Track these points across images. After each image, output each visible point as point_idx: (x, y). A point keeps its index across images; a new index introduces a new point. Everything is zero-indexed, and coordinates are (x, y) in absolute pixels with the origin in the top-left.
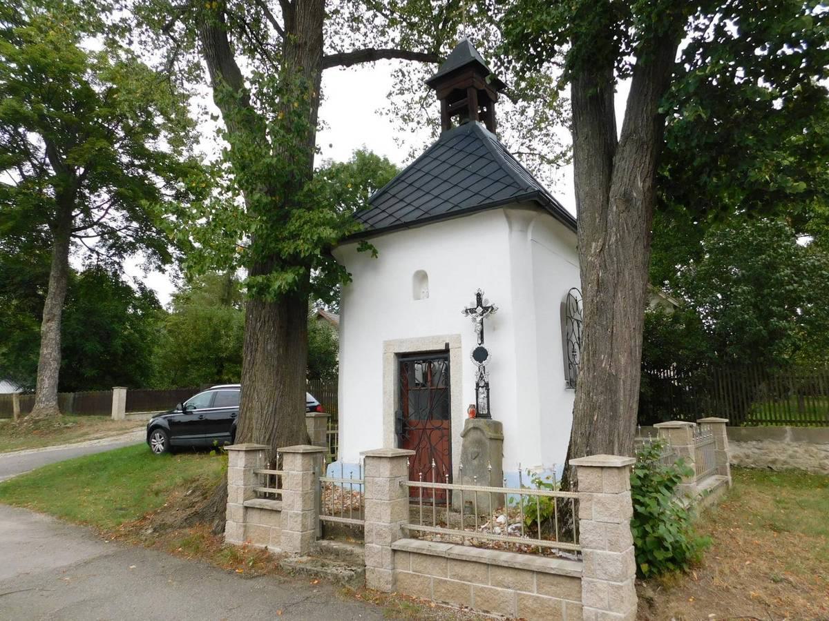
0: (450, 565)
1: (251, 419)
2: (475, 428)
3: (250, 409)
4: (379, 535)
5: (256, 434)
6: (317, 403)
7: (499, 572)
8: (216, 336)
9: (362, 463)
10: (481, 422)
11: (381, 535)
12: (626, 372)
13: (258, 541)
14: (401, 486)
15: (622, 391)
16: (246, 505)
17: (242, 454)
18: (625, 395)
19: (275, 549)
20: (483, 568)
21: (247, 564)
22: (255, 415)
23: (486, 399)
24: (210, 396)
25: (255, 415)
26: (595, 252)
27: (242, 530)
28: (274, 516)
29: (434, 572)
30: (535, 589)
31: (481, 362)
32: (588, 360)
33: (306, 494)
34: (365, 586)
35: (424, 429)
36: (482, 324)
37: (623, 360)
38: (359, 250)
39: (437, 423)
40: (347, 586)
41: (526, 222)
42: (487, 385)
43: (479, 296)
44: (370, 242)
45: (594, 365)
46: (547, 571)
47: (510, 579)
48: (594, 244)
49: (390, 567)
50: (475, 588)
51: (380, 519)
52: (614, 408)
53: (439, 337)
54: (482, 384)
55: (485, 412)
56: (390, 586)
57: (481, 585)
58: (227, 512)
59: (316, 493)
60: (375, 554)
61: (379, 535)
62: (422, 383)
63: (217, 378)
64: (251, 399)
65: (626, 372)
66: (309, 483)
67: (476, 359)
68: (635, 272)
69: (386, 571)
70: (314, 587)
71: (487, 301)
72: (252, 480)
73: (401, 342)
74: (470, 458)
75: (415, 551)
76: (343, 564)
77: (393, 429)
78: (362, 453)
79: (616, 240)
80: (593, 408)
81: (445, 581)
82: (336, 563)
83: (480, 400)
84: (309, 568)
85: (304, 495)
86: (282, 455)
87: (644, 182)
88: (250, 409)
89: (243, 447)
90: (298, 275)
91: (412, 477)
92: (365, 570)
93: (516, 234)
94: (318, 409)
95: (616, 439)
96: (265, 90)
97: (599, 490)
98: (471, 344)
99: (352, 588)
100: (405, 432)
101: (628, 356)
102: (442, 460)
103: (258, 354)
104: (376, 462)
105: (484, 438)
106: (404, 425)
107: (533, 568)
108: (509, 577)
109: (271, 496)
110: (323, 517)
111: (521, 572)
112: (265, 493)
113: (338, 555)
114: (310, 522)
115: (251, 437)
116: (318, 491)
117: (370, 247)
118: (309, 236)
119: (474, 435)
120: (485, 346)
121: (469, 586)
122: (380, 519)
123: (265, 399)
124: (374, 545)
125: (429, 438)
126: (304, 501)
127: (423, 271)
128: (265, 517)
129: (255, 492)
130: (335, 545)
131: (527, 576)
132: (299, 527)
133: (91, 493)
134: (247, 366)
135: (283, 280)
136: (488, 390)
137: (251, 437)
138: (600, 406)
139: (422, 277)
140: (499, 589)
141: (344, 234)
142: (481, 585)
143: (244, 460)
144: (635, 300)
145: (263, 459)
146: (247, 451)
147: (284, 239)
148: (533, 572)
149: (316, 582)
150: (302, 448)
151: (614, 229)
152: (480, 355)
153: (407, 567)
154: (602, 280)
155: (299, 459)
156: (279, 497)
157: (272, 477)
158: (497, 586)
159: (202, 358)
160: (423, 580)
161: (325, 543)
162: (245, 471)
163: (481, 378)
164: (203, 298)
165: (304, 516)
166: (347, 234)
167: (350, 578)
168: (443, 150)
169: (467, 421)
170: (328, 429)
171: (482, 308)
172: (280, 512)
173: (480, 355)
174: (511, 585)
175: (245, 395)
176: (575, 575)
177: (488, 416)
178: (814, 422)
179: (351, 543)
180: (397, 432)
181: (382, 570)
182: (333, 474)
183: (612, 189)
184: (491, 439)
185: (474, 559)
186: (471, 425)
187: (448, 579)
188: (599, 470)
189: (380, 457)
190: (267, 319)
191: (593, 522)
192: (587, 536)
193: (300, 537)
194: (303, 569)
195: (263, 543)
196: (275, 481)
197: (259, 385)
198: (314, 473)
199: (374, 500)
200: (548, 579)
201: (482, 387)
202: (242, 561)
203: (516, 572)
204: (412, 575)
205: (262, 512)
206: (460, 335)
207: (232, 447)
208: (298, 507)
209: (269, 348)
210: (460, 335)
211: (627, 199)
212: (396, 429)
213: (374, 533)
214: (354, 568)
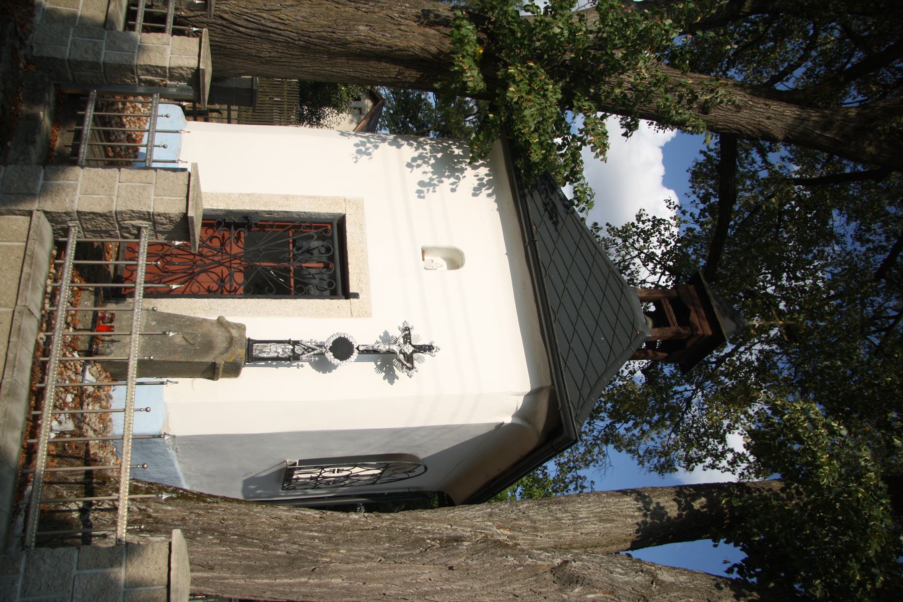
9: (181, 166)
18: (283, 585)
23: (275, 355)
31: (331, 349)
43: (429, 348)
51: (86, 193)
52: (265, 570)
62: (301, 255)
65: (319, 586)
67: (335, 342)
71: (422, 360)
77: (233, 207)
78: (195, 166)
83: (273, 347)
86: (198, 34)
96: (591, 36)
105: (216, 352)
112: (137, 6)
122: (86, 193)
123: (285, 17)
127: (462, 265)
132: (77, 56)
133: (313, 547)
152: (343, 348)
157: (162, 19)
180: (230, 213)
182: (170, 114)
191: (75, 572)
192: (48, 561)
193: (59, 56)
201: (293, 350)
206: (370, 315)
209: (361, 28)
210: (370, 315)
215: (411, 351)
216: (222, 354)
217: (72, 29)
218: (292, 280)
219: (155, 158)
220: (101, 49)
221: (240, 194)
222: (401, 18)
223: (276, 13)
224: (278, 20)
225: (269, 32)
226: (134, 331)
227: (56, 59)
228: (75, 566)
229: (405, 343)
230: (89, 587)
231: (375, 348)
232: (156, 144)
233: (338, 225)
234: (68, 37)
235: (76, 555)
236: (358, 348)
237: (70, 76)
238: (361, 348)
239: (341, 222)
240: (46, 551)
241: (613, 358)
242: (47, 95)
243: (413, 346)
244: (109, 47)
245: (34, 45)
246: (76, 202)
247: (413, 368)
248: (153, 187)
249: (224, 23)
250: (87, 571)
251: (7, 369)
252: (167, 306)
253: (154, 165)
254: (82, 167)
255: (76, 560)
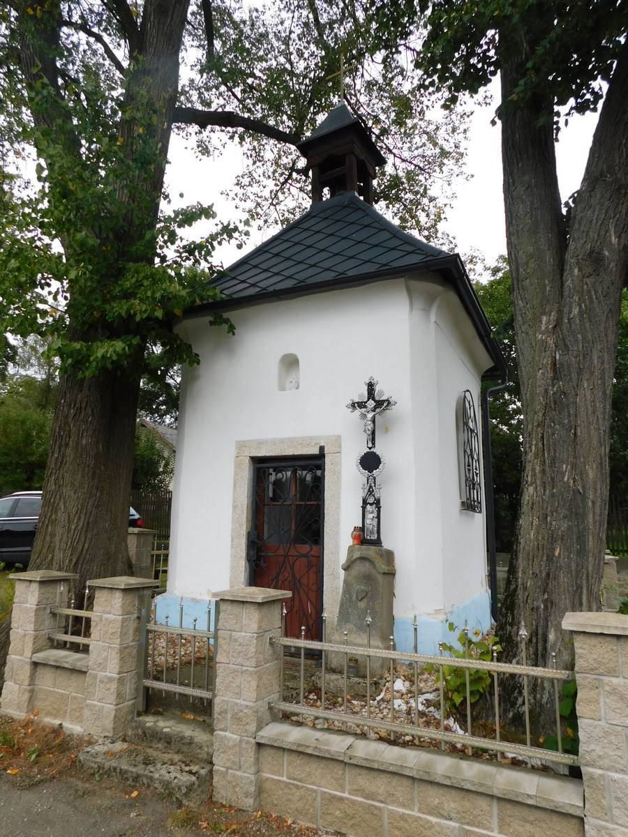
0: (349, 774)
1: (53, 535)
2: (362, 559)
3: (53, 523)
4: (237, 719)
5: (59, 555)
6: (137, 516)
7: (432, 792)
8: (28, 440)
10: (371, 551)
11: (240, 719)
12: (595, 490)
13: (49, 714)
14: (271, 644)
15: (591, 516)
16: (34, 659)
17: (35, 586)
18: (595, 522)
19: (74, 728)
20: (406, 782)
21: (27, 758)
22: (59, 531)
24: (11, 503)
25: (59, 531)
26: (547, 328)
27: (27, 696)
28: (75, 680)
29: (323, 783)
30: (495, 821)
31: (371, 471)
32: (543, 472)
33: (125, 648)
34: (211, 798)
35: (286, 556)
36: (374, 421)
37: (591, 474)
38: (211, 323)
39: (305, 548)
40: (185, 802)
41: (430, 299)
42: (377, 503)
43: (371, 387)
44: (225, 315)
45: (553, 479)
46: (520, 800)
47: (453, 805)
48: (544, 319)
49: (253, 770)
50: (391, 812)
51: (239, 695)
53: (311, 438)
54: (371, 500)
55: (375, 537)
56: (251, 801)
57: (401, 810)
58: (7, 669)
59: (140, 646)
60: (229, 744)
61: (237, 719)
62: (286, 497)
63: (27, 484)
64: (55, 510)
65: (595, 490)
66: (131, 632)
67: (364, 468)
68: (606, 356)
69: (246, 775)
70: (132, 805)
71: (382, 393)
72: (47, 623)
73: (260, 443)
74: (354, 598)
75: (294, 748)
76: (177, 758)
77: (244, 554)
78: (214, 595)
79: (580, 311)
80: (553, 540)
81: (341, 799)
82: (167, 757)
83: (368, 521)
84: (124, 767)
85: (122, 651)
87: (619, 237)
88: (53, 523)
89: (37, 575)
90: (129, 346)
91: (290, 631)
92: (211, 771)
93: (418, 314)
94: (139, 522)
95: (584, 582)
97: (612, 672)
98: (354, 449)
99: (192, 804)
100: (261, 563)
101: (597, 468)
102: (307, 595)
103: (69, 451)
104: (236, 609)
105: (374, 572)
106: (259, 550)
107: (496, 792)
108: (451, 803)
109: (76, 648)
110: (150, 683)
111: (471, 795)
112: (65, 642)
113: (169, 743)
114: (129, 689)
115: (52, 559)
116: (143, 629)
117: (227, 321)
118: (149, 294)
119: (359, 568)
120: (377, 450)
121: (379, 809)
122: (239, 695)
123: (75, 509)
124: (228, 734)
125: (292, 569)
126: (122, 659)
128: (62, 678)
129: (51, 639)
130: (166, 725)
131: (483, 803)
134: (53, 466)
135: (109, 349)
136: (379, 508)
137: (52, 559)
138: (563, 536)
139: (290, 363)
140: (433, 819)
141: (194, 301)
142: (401, 810)
143: (37, 594)
144: (604, 393)
145: (66, 593)
146: (42, 583)
147: (114, 298)
148: (492, 797)
149: (135, 794)
150: (123, 581)
151: (576, 298)
152: (370, 462)
153: (279, 773)
154: (562, 364)
155: (118, 599)
156: (85, 649)
157: (77, 619)
158: (430, 813)
159: (11, 463)
160: (304, 792)
161: (149, 721)
162: (37, 610)
163: (371, 492)
164: (19, 402)
165: (121, 681)
166: (198, 302)
167: (190, 788)
168: (312, 222)
169: (351, 550)
170: (153, 550)
171: (374, 403)
172: (85, 673)
173: (370, 462)
174: (453, 815)
175: (46, 502)
176: (571, 811)
177: (378, 542)
178: (621, 551)
179: (187, 722)
180: (249, 558)
181: (239, 773)
182: (165, 609)
183: (572, 246)
184: (384, 574)
185: (391, 769)
186: (357, 555)
187: (346, 795)
188: (614, 640)
189: (243, 602)
190: (83, 405)
191: (602, 723)
192: (592, 747)
193: (113, 713)
194: (115, 769)
195: (56, 717)
196: (81, 626)
197: (67, 491)
198: (139, 618)
199: (231, 666)
200: (518, 811)
201: (371, 504)
202: (19, 750)
203: (463, 794)
204: (287, 784)
205: (59, 672)
206: (339, 437)
207: (22, 575)
208: (112, 669)
209: (84, 442)
210: (339, 437)
211: (595, 259)
212: (248, 554)
213: (229, 716)
214: (195, 768)
215: (373, 402)
216: (375, 567)
217: (88, 701)
218: (308, 503)
219: (205, 629)
220: (106, 676)
221: (232, 547)
222: (75, 406)
223: (72, 516)
224: (78, 515)
225: (88, 523)
226: (366, 653)
227: (115, 716)
228: (597, 722)
229: (365, 407)
230: (618, 711)
231: (370, 433)
232: (192, 627)
233: (259, 463)
234: (95, 706)
235: (586, 721)
236: (370, 448)
237: (130, 702)
238: (370, 445)
239: (256, 461)
240: (582, 748)
241: (375, 225)
242: (148, 725)
243: (375, 401)
244: (104, 669)
245: (103, 735)
246: (248, 703)
247: (388, 400)
248: (234, 633)
249: (81, 562)
250: (603, 712)
251: (404, 773)
252: (331, 610)
253: (212, 629)
254: (214, 696)
255: (591, 721)
